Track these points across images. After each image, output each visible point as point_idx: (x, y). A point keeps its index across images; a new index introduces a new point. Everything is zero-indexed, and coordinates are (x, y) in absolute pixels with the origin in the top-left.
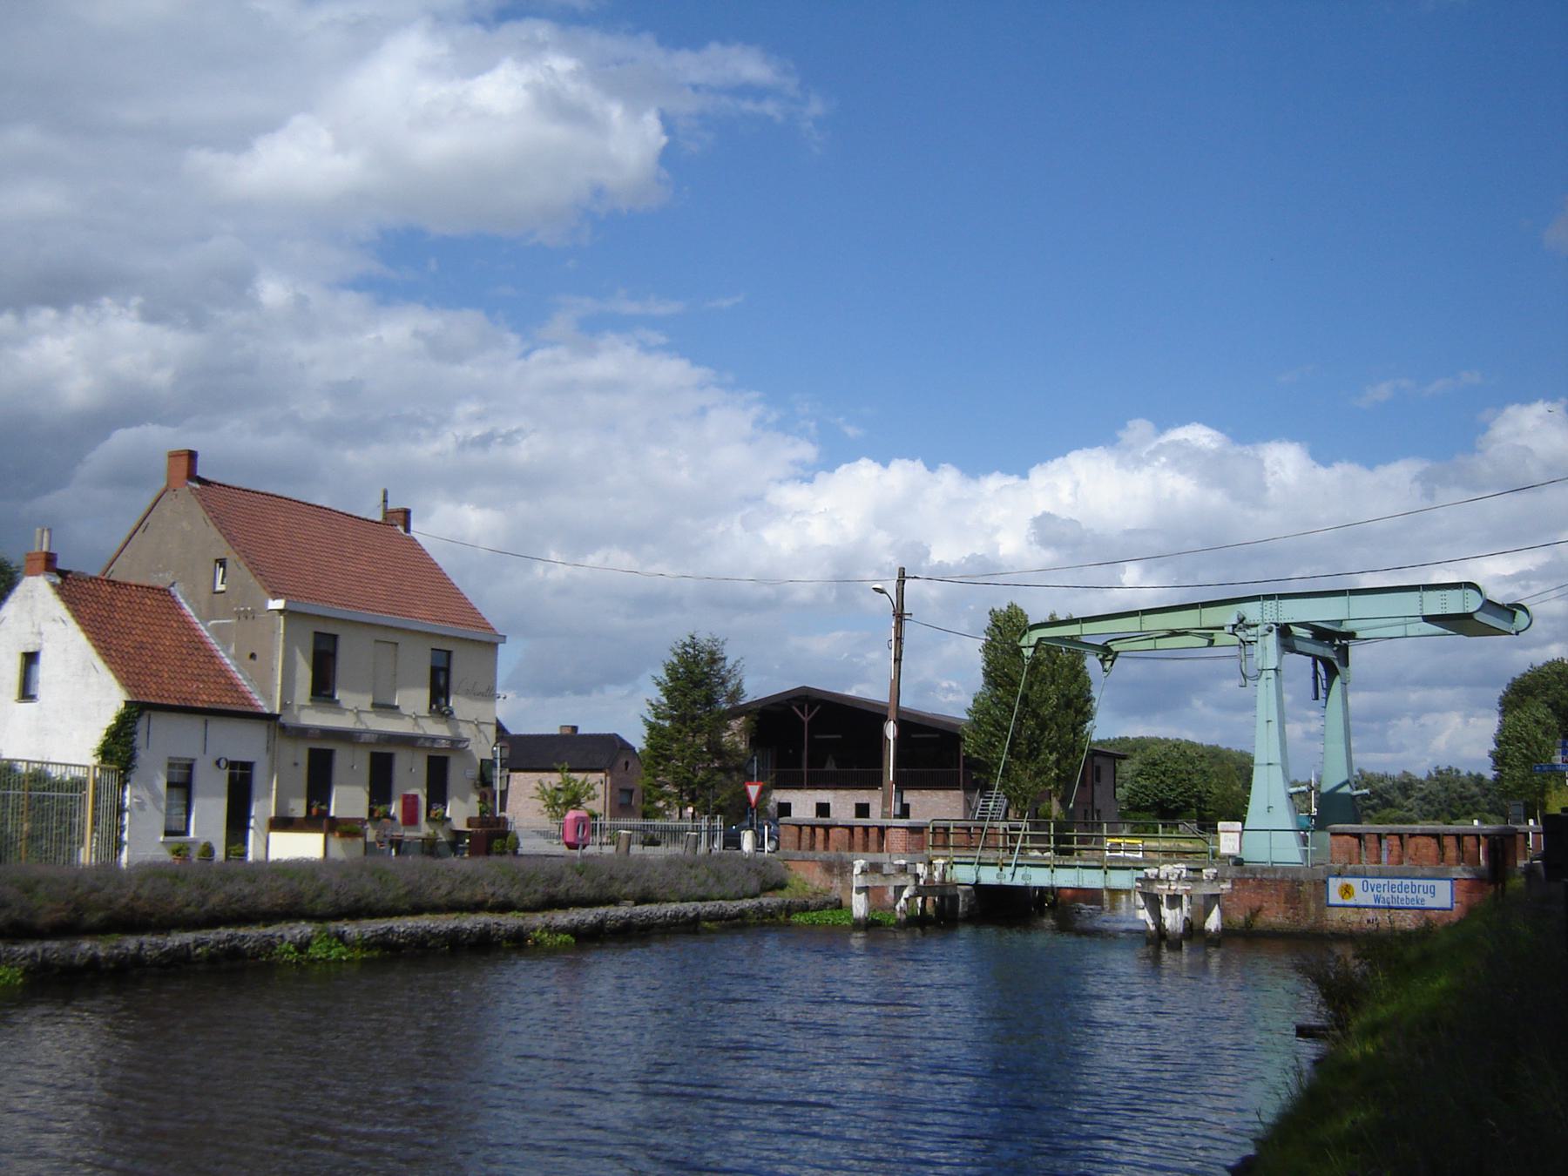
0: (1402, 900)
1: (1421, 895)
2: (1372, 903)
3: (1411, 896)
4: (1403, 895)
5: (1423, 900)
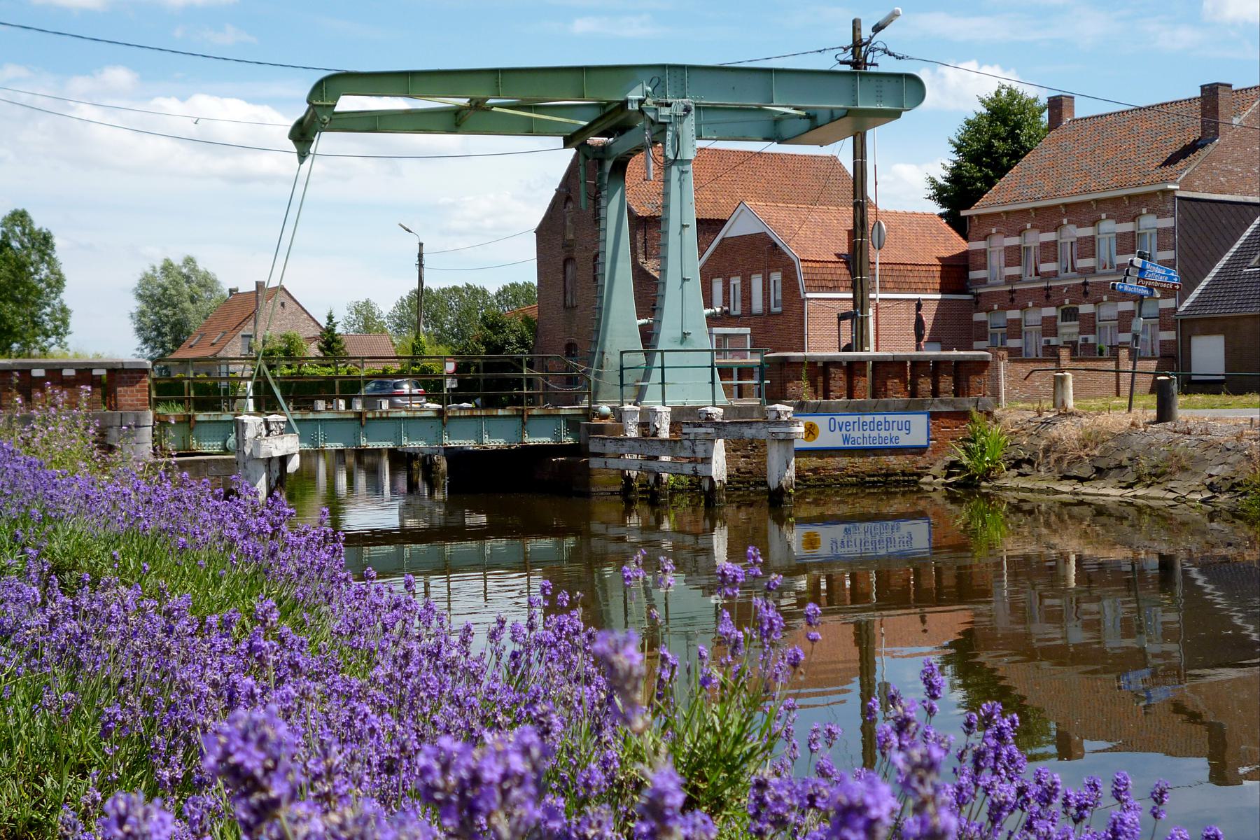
0: (874, 439)
1: (895, 433)
2: (840, 444)
3: (884, 434)
4: (875, 434)
5: (897, 438)
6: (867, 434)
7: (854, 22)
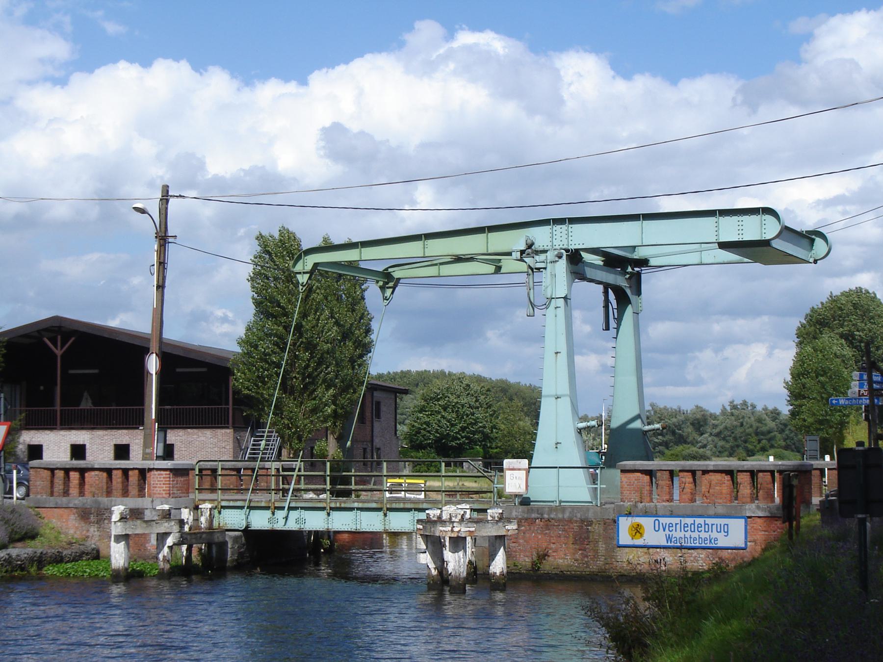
0: (695, 539)
1: (714, 535)
2: (664, 543)
3: (703, 535)
4: (695, 535)
5: (716, 539)
6: (688, 535)
7: (176, 236)
